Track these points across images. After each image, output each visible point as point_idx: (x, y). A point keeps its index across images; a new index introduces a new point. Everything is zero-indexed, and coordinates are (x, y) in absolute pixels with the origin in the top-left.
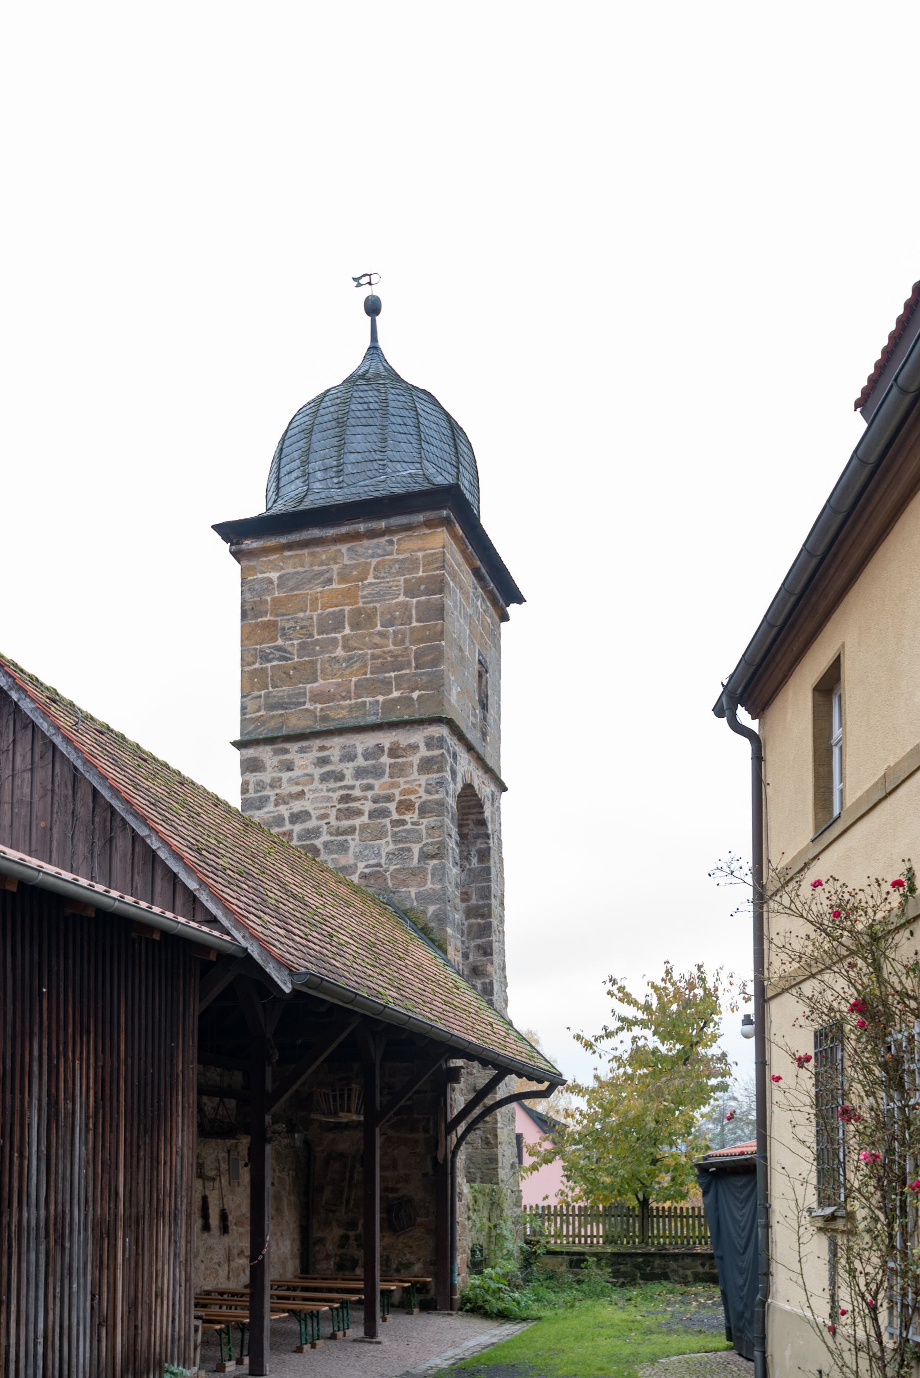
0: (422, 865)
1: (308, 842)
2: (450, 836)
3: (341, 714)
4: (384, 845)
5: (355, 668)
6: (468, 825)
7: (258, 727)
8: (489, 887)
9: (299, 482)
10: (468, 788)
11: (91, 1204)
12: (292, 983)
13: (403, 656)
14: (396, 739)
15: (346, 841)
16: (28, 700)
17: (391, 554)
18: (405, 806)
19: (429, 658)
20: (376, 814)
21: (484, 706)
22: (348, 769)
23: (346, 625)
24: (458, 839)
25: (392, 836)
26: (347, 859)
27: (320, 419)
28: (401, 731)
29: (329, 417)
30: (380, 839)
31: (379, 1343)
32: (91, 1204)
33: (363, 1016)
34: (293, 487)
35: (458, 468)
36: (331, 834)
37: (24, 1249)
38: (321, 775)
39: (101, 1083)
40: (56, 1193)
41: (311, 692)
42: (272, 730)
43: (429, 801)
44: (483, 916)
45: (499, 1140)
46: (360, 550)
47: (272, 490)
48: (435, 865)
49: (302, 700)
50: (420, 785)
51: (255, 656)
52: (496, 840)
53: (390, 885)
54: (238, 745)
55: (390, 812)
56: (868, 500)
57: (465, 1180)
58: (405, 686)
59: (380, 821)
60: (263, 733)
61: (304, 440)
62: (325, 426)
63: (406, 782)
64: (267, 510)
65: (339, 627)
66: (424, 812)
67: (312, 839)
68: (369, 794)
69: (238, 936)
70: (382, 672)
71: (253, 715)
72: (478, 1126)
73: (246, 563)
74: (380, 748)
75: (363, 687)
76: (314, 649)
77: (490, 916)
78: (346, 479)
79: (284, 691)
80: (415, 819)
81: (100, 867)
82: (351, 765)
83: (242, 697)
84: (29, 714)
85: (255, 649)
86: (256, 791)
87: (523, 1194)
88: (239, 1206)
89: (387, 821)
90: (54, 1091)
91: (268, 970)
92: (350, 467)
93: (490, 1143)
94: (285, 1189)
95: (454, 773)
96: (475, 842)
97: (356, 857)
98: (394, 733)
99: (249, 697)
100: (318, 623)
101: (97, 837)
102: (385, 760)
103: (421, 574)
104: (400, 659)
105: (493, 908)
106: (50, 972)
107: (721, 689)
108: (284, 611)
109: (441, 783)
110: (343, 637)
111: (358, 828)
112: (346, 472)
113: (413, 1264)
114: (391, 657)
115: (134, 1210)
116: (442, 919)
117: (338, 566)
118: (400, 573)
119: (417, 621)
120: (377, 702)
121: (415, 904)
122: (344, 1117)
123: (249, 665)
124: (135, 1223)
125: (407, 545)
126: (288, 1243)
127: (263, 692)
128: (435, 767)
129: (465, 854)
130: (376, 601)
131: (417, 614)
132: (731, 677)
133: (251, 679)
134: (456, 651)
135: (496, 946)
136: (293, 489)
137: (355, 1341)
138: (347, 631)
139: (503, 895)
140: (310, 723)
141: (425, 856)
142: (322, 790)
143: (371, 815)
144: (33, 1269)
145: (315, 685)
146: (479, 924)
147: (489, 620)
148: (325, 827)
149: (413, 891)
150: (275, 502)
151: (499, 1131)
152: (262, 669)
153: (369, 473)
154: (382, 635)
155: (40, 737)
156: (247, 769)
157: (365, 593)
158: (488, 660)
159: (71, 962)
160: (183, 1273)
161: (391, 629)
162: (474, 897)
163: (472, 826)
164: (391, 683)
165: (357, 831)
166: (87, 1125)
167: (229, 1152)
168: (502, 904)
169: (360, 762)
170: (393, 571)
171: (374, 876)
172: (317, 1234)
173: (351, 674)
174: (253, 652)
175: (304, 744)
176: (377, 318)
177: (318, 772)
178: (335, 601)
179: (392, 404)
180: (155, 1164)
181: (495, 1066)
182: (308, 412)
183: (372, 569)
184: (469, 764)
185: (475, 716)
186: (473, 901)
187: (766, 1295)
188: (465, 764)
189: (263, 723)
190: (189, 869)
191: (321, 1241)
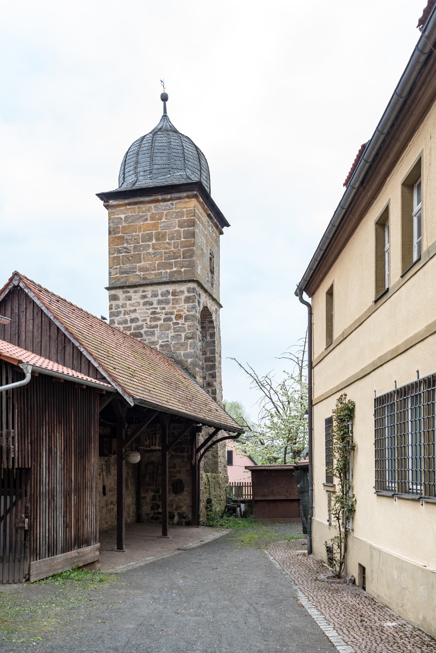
0: (186, 341)
1: (138, 331)
2: (197, 329)
3: (152, 276)
4: (170, 333)
7: (117, 281)
8: (214, 349)
10: (206, 308)
12: (134, 402)
14: (175, 288)
15: (154, 331)
16: (32, 292)
17: (173, 209)
18: (179, 317)
19: (188, 254)
21: (212, 272)
22: (155, 300)
23: (154, 239)
26: (155, 339)
28: (177, 285)
29: (146, 148)
30: (168, 330)
31: (168, 538)
34: (131, 178)
35: (201, 172)
36: (148, 328)
39: (66, 441)
41: (139, 267)
42: (122, 283)
44: (212, 361)
46: (159, 207)
49: (135, 270)
50: (185, 308)
51: (115, 251)
53: (172, 350)
54: (108, 289)
55: (172, 319)
56: (338, 234)
58: (178, 266)
59: (168, 323)
61: (135, 158)
62: (144, 152)
63: (179, 307)
64: (119, 187)
65: (150, 240)
66: (187, 320)
68: (164, 311)
69: (114, 384)
71: (114, 276)
73: (110, 210)
74: (168, 292)
75: (161, 266)
76: (140, 249)
77: (215, 361)
80: (183, 322)
81: (60, 357)
82: (156, 299)
83: (109, 268)
84: (32, 298)
85: (115, 248)
86: (116, 309)
87: (229, 477)
88: (110, 484)
89: (171, 323)
90: (50, 445)
91: (125, 397)
92: (155, 170)
93: (215, 456)
94: (129, 476)
95: (199, 303)
97: (158, 338)
99: (112, 268)
100: (142, 238)
101: (59, 345)
102: (170, 297)
103: (185, 218)
104: (176, 254)
105: (216, 358)
106: (48, 402)
107: (297, 287)
108: (127, 232)
109: (193, 308)
110: (152, 244)
112: (153, 173)
113: (182, 507)
114: (173, 253)
117: (150, 213)
119: (184, 238)
120: (167, 272)
121: (183, 358)
122: (153, 448)
123: (112, 254)
125: (179, 206)
126: (130, 499)
127: (118, 267)
128: (191, 301)
129: (205, 335)
130: (166, 229)
131: (183, 235)
132: (300, 283)
133: (113, 261)
134: (200, 251)
135: (217, 374)
136: (130, 179)
137: (158, 537)
138: (154, 241)
139: (221, 352)
140: (139, 280)
141: (187, 338)
142: (144, 309)
143: (164, 320)
145: (140, 264)
146: (210, 365)
147: (214, 235)
148: (145, 325)
149: (182, 352)
150: (123, 184)
151: (219, 451)
154: (169, 244)
155: (36, 308)
156: (112, 299)
157: (161, 225)
159: (55, 398)
161: (172, 241)
163: (207, 323)
164: (172, 264)
166: (61, 456)
167: (106, 462)
168: (220, 356)
169: (160, 297)
170: (173, 216)
171: (165, 346)
172: (143, 495)
173: (156, 260)
174: (114, 249)
175: (136, 289)
176: (167, 102)
177: (142, 301)
179: (173, 143)
181: (215, 427)
182: (137, 145)
183: (164, 216)
185: (208, 277)
186: (208, 355)
187: (312, 516)
188: (204, 298)
189: (119, 280)
190: (95, 359)
191: (144, 498)
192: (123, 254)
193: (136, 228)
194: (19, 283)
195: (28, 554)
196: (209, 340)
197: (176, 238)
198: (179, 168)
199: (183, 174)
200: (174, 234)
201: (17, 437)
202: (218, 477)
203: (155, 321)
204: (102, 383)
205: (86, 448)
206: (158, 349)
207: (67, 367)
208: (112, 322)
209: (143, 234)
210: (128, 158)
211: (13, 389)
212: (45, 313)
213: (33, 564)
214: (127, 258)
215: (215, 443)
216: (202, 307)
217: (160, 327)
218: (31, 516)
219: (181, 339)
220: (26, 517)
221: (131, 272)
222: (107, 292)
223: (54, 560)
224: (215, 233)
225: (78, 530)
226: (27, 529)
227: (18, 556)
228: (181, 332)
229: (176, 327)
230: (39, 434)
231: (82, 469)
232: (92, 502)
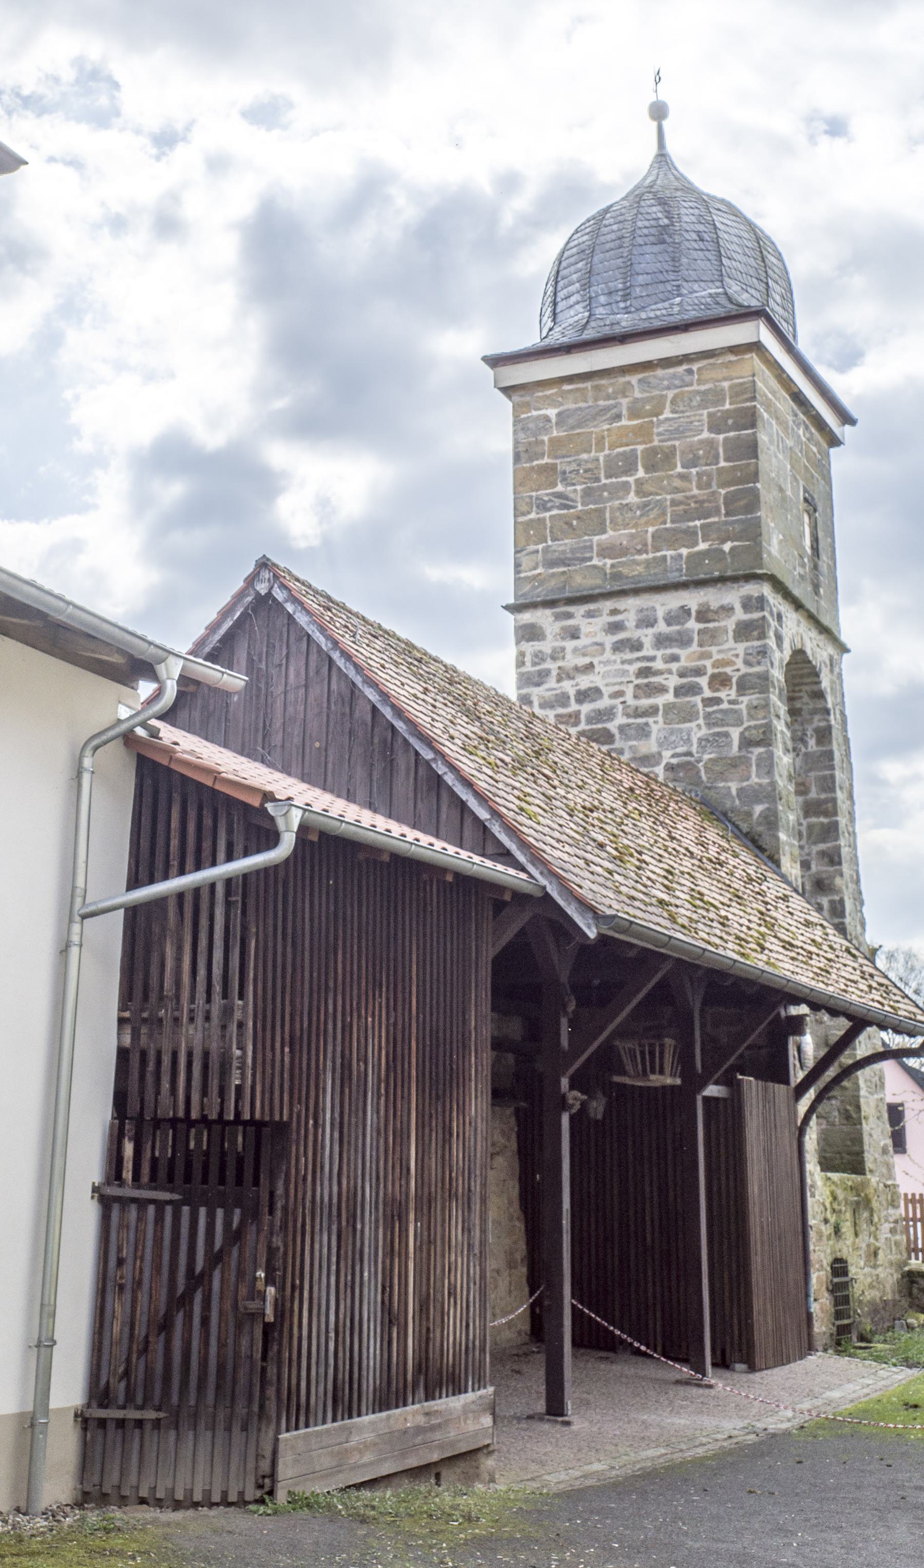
0: (743, 753)
1: (600, 726)
2: (778, 717)
4: (695, 729)
5: (652, 516)
6: (801, 697)
8: (833, 777)
9: (579, 308)
10: (799, 658)
11: (382, 1180)
13: (709, 502)
14: (705, 599)
15: (647, 724)
17: (691, 384)
18: (719, 681)
19: (742, 503)
20: (683, 690)
22: (647, 636)
24: (789, 719)
25: (704, 718)
26: (650, 746)
27: (602, 239)
29: (613, 236)
30: (690, 721)
32: (382, 1180)
33: (679, 960)
35: (767, 284)
36: (628, 716)
37: (317, 1227)
38: (614, 644)
40: (348, 1165)
41: (598, 545)
42: (552, 590)
43: (750, 674)
44: (826, 814)
45: (863, 1114)
47: (547, 315)
48: (760, 754)
49: (588, 555)
50: (737, 656)
52: (838, 716)
53: (704, 778)
55: (701, 688)
57: (818, 1168)
58: (714, 536)
60: (541, 594)
62: (608, 246)
63: (720, 652)
65: (630, 469)
67: (604, 721)
68: (674, 666)
70: (685, 521)
71: (529, 574)
72: (831, 1094)
75: (663, 539)
76: (601, 496)
77: (835, 813)
78: (635, 303)
79: (565, 544)
82: (650, 631)
83: (516, 552)
85: (531, 497)
89: (697, 700)
90: (347, 1052)
92: (638, 289)
95: (779, 638)
96: (812, 719)
97: (660, 745)
98: (702, 593)
100: (605, 466)
102: (693, 625)
103: (727, 406)
104: (706, 505)
105: (839, 802)
106: (344, 919)
108: (564, 452)
110: (637, 481)
111: (661, 708)
114: (696, 502)
115: (426, 1190)
116: (771, 821)
118: (703, 405)
119: (726, 460)
120: (680, 556)
121: (737, 802)
123: (523, 514)
124: (426, 1203)
127: (540, 547)
128: (755, 633)
129: (799, 733)
130: (675, 439)
131: (725, 451)
133: (526, 531)
134: (775, 493)
135: (845, 851)
136: (574, 314)
138: (641, 473)
139: (851, 785)
140: (599, 582)
141: (747, 743)
142: (615, 662)
144: (325, 1250)
145: (604, 537)
146: (822, 824)
147: (815, 449)
149: (734, 787)
150: (551, 330)
151: (862, 1101)
152: (539, 519)
153: (661, 296)
157: (661, 429)
158: (815, 496)
160: (478, 1268)
161: (694, 471)
162: (814, 789)
163: (806, 699)
164: (696, 533)
165: (661, 712)
168: (851, 797)
169: (662, 627)
170: (694, 403)
173: (647, 523)
174: (527, 500)
175: (592, 606)
178: (624, 440)
179: (686, 219)
180: (447, 1137)
181: (849, 1017)
182: (588, 230)
184: (798, 625)
185: (803, 565)
186: (813, 794)
192: (555, 512)
193: (590, 441)
194: (272, 588)
195: (272, 1406)
196: (815, 748)
197: (702, 461)
198: (704, 278)
199: (717, 294)
200: (698, 449)
201: (251, 1024)
202: (865, 1185)
203: (649, 696)
204: (500, 867)
205: (452, 1069)
206: (661, 779)
207: (399, 820)
208: (526, 700)
209: (608, 456)
210: (564, 264)
211: (245, 876)
212: (339, 669)
213: (286, 1440)
214: (566, 523)
215: (848, 1071)
216: (787, 654)
217: (666, 713)
218: (284, 1277)
219: (730, 744)
220: (269, 1280)
221: (578, 559)
222: (510, 619)
223: (349, 1431)
224: (817, 444)
225: (425, 1339)
226: (272, 1320)
227: (241, 1409)
228: (728, 725)
229: (714, 712)
230: (314, 1018)
231: (440, 1136)
232: (469, 1245)
